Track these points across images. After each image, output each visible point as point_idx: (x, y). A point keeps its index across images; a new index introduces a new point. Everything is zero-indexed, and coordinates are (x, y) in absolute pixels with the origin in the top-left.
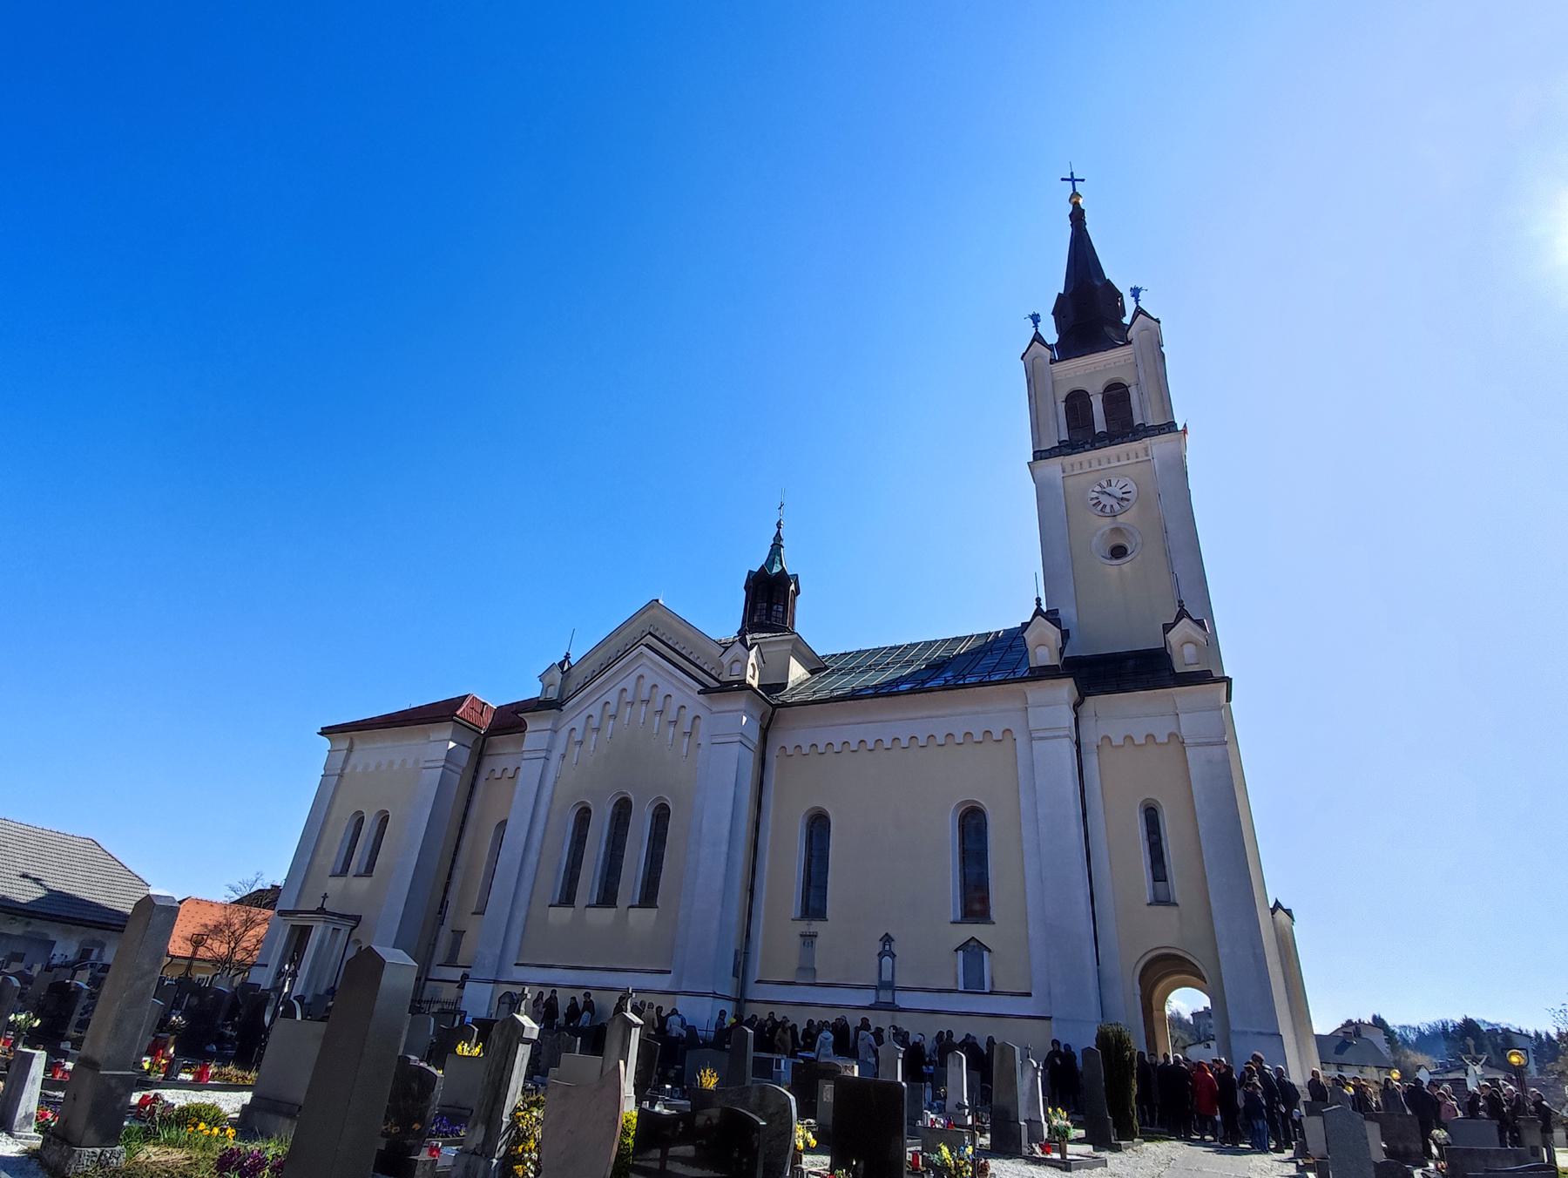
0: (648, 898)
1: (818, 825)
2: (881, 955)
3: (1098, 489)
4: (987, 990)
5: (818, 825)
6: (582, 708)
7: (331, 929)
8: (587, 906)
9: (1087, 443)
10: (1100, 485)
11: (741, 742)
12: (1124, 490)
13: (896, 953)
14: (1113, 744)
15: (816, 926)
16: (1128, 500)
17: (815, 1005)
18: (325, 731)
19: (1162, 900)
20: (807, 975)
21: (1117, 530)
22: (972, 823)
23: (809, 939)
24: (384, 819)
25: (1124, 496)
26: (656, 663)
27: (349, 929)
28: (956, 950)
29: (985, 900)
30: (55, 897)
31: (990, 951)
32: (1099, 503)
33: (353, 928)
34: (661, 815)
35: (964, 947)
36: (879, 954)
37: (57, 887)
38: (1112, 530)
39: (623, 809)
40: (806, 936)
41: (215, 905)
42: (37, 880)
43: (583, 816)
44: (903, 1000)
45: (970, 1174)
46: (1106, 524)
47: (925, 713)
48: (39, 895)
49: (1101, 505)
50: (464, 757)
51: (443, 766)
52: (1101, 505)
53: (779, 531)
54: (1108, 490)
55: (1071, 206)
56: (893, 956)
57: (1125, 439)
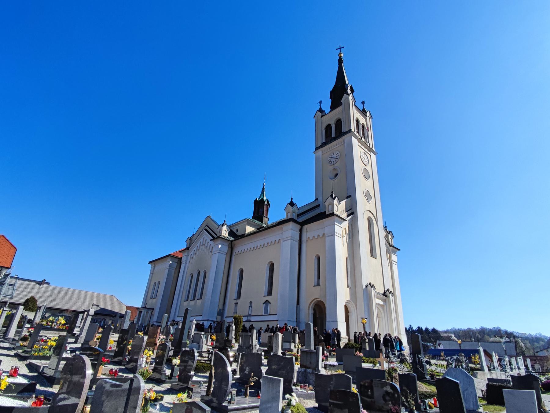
1: (242, 272)
2: (249, 307)
4: (268, 314)
7: (146, 312)
9: (329, 142)
10: (331, 155)
11: (219, 252)
13: (252, 306)
18: (150, 263)
21: (334, 169)
23: (236, 304)
24: (159, 282)
26: (200, 236)
27: (151, 312)
30: (102, 309)
31: (270, 303)
33: (152, 312)
36: (249, 307)
37: (102, 307)
41: (68, 310)
42: (98, 306)
44: (252, 319)
46: (331, 167)
47: (264, 238)
48: (97, 309)
50: (175, 265)
51: (169, 268)
53: (264, 186)
54: (333, 156)
55: (339, 57)
56: (252, 307)
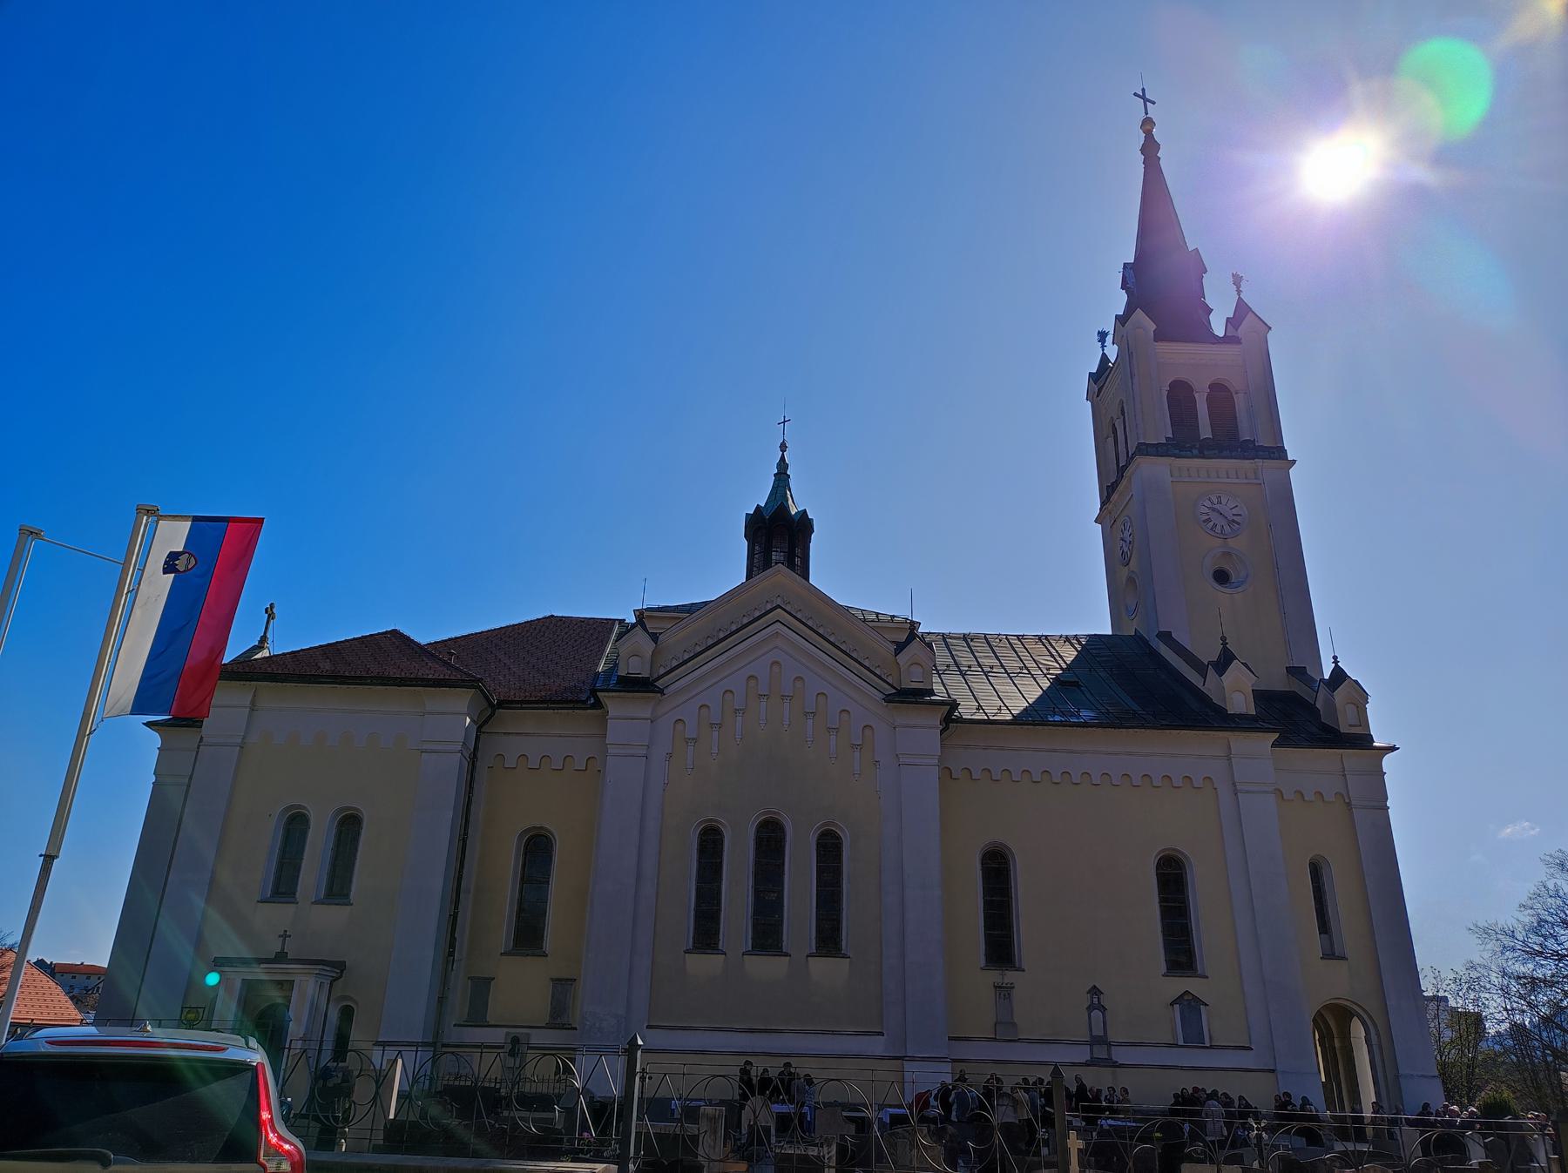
0: (829, 940)
1: (537, 848)
2: (1091, 1008)
3: (1208, 504)
5: (537, 848)
6: (691, 695)
8: (808, 956)
12: (1234, 511)
14: (1306, 798)
15: (1010, 976)
16: (1238, 523)
17: (1012, 1062)
19: (1330, 954)
20: (1005, 1030)
21: (1227, 554)
22: (997, 867)
23: (1004, 991)
24: (349, 826)
25: (1235, 518)
28: (1172, 1004)
29: (1190, 953)
31: (1206, 1005)
32: (1209, 520)
34: (829, 847)
35: (1178, 1000)
36: (1088, 1008)
38: (1224, 553)
39: (770, 838)
40: (1000, 987)
43: (710, 842)
44: (1120, 1055)
45: (618, 1151)
49: (1212, 523)
52: (1212, 523)
54: (1217, 506)
56: (1103, 1009)
57: (1233, 454)
